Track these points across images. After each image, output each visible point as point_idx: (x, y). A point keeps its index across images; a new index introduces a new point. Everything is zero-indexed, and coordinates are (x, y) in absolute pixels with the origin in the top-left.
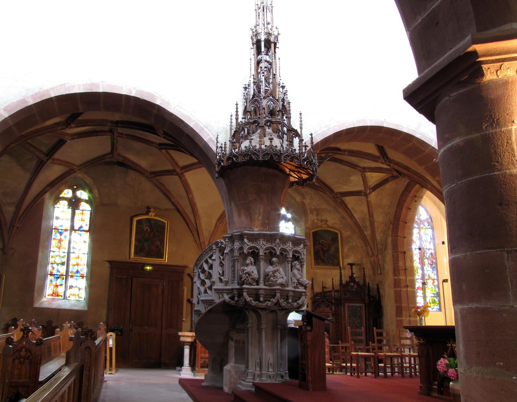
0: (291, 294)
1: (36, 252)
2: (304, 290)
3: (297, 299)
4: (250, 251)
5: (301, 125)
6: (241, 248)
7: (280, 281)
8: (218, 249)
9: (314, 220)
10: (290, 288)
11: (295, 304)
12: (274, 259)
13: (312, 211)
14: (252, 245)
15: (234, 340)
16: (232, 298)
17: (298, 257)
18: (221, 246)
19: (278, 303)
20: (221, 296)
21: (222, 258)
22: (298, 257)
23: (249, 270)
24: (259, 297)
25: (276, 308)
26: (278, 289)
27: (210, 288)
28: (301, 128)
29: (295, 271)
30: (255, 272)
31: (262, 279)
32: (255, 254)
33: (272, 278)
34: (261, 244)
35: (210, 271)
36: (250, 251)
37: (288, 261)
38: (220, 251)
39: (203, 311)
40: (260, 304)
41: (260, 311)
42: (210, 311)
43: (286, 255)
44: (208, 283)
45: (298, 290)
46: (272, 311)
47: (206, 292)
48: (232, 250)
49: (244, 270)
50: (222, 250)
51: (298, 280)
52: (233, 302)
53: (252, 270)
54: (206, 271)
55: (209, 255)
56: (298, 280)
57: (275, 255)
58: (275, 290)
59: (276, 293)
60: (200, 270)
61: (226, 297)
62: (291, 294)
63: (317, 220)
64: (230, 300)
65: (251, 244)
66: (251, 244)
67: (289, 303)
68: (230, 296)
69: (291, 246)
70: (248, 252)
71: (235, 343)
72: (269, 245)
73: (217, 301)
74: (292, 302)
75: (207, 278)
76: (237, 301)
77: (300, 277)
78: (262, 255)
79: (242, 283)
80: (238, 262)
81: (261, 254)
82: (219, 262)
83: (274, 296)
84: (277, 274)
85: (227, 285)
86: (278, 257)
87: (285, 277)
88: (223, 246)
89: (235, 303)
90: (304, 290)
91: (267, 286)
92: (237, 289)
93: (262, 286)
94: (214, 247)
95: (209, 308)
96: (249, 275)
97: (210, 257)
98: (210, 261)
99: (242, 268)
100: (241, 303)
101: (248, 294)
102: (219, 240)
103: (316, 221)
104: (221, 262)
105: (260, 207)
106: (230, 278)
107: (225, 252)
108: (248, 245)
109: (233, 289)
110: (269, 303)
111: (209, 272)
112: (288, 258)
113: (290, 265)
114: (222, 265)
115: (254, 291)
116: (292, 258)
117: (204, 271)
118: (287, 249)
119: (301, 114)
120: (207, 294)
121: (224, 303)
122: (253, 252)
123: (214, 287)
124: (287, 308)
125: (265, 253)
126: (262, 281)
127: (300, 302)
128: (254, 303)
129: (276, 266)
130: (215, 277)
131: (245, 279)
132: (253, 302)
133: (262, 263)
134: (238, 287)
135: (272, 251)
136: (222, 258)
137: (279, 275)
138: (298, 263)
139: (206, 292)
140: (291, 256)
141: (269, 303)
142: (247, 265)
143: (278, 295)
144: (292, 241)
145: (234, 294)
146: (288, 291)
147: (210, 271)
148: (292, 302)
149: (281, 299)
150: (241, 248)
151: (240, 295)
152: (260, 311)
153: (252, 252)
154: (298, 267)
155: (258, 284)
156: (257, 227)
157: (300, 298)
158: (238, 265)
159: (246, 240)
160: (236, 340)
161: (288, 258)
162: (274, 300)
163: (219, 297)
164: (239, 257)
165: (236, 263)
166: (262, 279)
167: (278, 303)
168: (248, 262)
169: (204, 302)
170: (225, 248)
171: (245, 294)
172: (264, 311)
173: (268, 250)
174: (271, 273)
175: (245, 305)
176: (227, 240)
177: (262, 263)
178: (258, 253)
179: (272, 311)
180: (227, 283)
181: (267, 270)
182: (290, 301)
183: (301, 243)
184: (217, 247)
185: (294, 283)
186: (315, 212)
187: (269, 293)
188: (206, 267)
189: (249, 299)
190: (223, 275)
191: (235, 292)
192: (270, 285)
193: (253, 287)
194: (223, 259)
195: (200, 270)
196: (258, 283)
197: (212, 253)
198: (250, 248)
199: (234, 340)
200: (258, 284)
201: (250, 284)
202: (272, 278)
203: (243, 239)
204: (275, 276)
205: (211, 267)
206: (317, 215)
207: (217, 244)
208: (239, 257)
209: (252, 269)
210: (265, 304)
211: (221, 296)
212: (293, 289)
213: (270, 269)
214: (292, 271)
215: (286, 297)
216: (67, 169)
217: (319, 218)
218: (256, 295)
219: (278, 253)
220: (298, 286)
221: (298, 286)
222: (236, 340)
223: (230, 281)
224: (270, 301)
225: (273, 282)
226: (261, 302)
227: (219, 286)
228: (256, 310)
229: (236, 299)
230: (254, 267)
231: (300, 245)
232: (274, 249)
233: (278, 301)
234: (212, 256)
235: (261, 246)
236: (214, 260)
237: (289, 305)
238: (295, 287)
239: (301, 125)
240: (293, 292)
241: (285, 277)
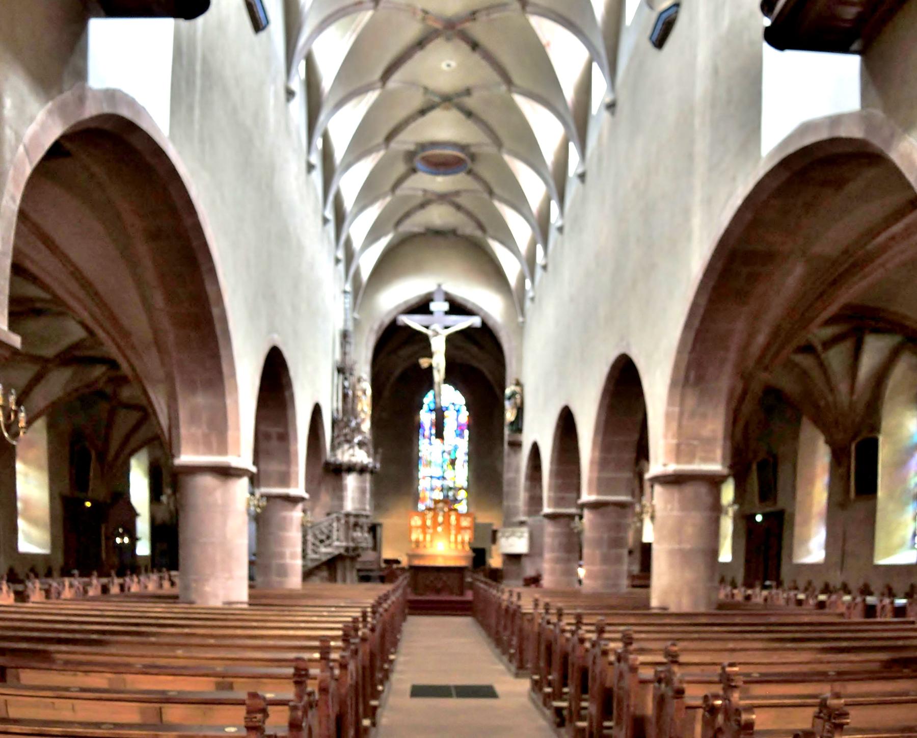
227: (336, 543)
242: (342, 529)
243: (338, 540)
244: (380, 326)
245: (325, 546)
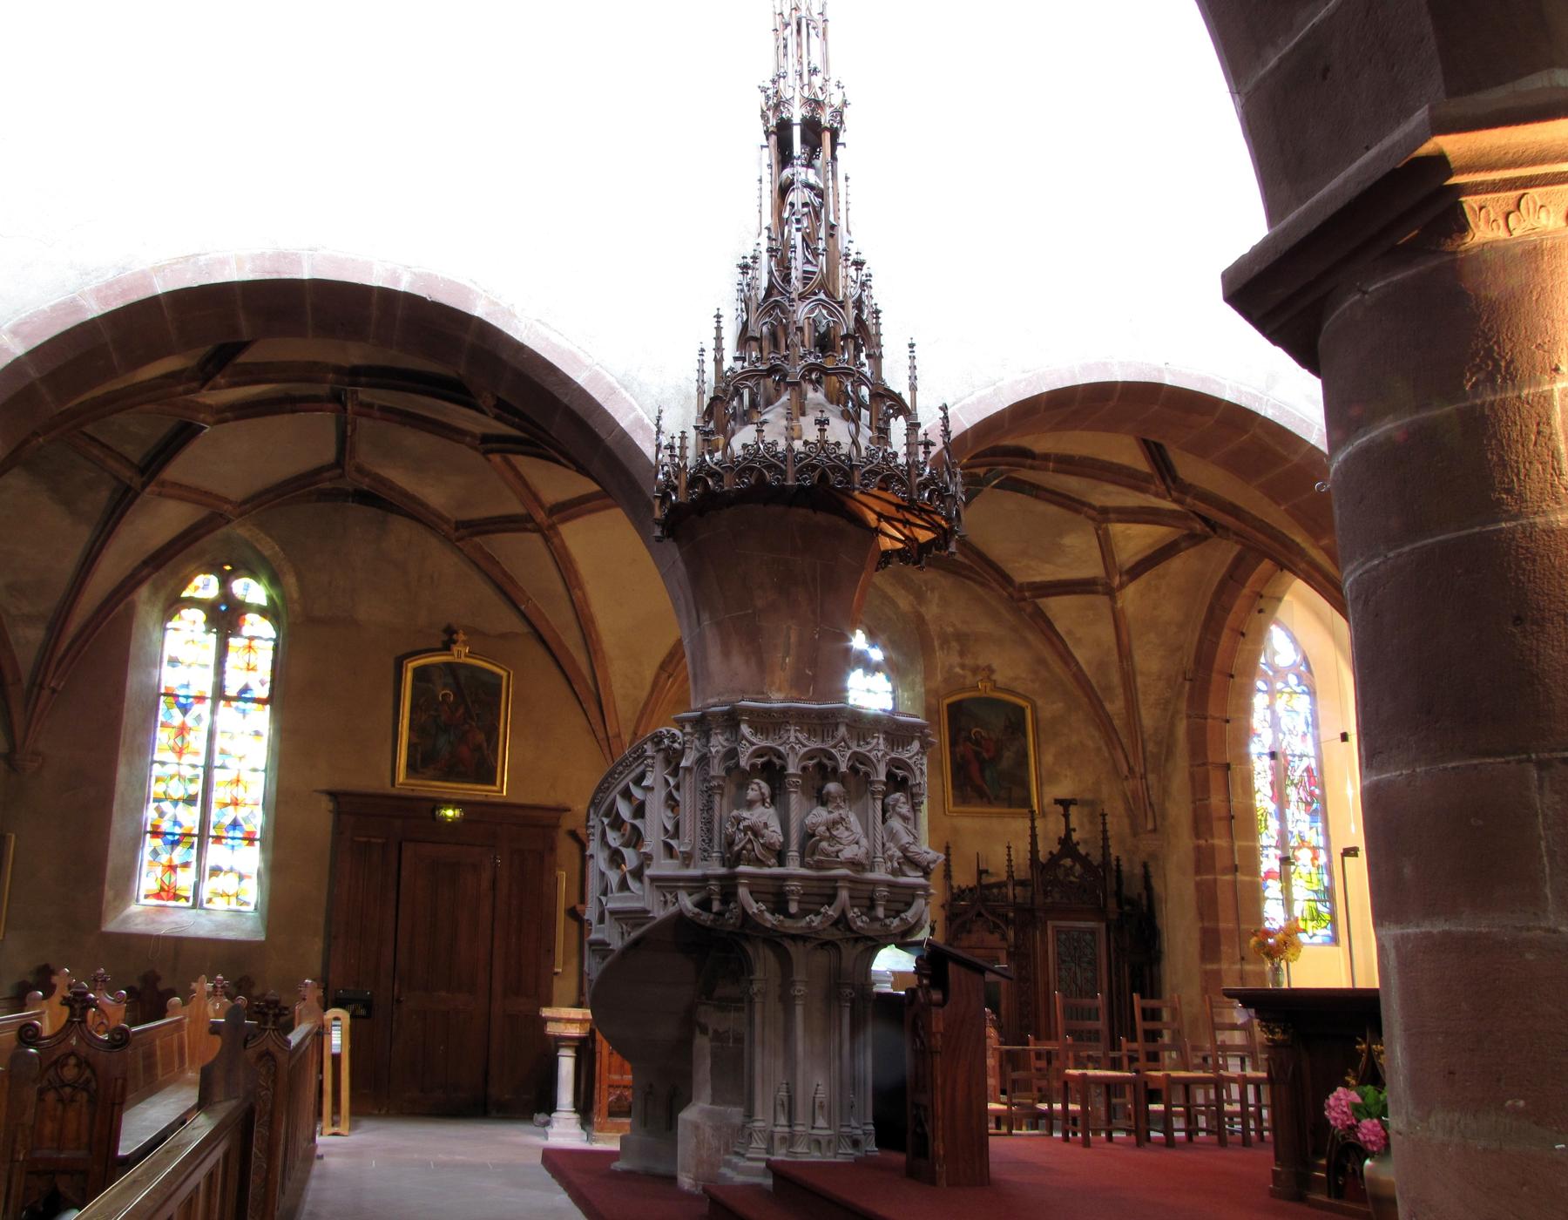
0: (883, 891)
2: (922, 881)
3: (900, 906)
4: (760, 761)
6: (732, 754)
7: (848, 852)
8: (661, 756)
10: (880, 874)
11: (896, 922)
12: (832, 787)
13: (945, 641)
14: (764, 744)
15: (711, 1032)
16: (704, 905)
17: (905, 779)
18: (669, 747)
19: (842, 921)
20: (669, 897)
21: (672, 781)
22: (905, 779)
23: (754, 819)
24: (787, 902)
25: (836, 935)
26: (844, 878)
27: (638, 874)
29: (896, 823)
30: (775, 825)
31: (794, 846)
32: (772, 771)
33: (824, 844)
34: (792, 739)
35: (637, 822)
36: (760, 761)
37: (873, 793)
38: (668, 761)
39: (617, 944)
40: (788, 923)
41: (787, 943)
42: (636, 943)
43: (867, 775)
44: (631, 857)
45: (902, 880)
46: (824, 945)
47: (623, 885)
48: (703, 760)
49: (739, 820)
50: (672, 759)
51: (904, 850)
52: (706, 918)
53: (764, 819)
54: (624, 821)
55: (633, 775)
56: (904, 850)
58: (835, 879)
59: (836, 889)
60: (606, 821)
61: (687, 902)
62: (883, 891)
63: (963, 666)
64: (697, 910)
65: (761, 742)
66: (761, 742)
67: (877, 919)
68: (696, 897)
69: (882, 747)
70: (753, 766)
71: (711, 1040)
72: (815, 744)
73: (660, 913)
74: (887, 917)
75: (627, 845)
76: (720, 914)
77: (911, 839)
78: (794, 775)
79: (733, 858)
80: (722, 795)
81: (791, 770)
82: (663, 794)
83: (831, 899)
84: (840, 832)
85: (688, 866)
86: (842, 779)
87: (864, 842)
88: (676, 745)
89: (714, 921)
90: (922, 881)
91: (810, 867)
92: (719, 878)
93: (793, 868)
94: (650, 749)
95: (634, 935)
96: (756, 834)
97: (638, 781)
98: (638, 793)
99: (735, 813)
100: (731, 918)
101: (751, 893)
102: (663, 730)
103: (958, 670)
104: (670, 796)
106: (699, 844)
107: (683, 764)
108: (752, 744)
109: (705, 878)
110: (817, 921)
111: (634, 827)
112: (872, 783)
113: (879, 804)
114: (672, 803)
115: (770, 882)
116: (885, 784)
117: (617, 823)
118: (871, 755)
120: (627, 894)
121: (680, 921)
122: (768, 766)
123: (648, 872)
124: (871, 934)
125: (804, 769)
126: (793, 853)
128: (770, 919)
129: (839, 807)
130: (653, 841)
131: (744, 848)
132: (768, 915)
133: (793, 797)
134: (722, 871)
135: (826, 761)
136: (672, 781)
137: (847, 833)
138: (903, 799)
139: (623, 885)
140: (883, 778)
141: (817, 921)
142: (750, 805)
143: (844, 895)
144: (885, 732)
145: (710, 893)
146: (875, 883)
147: (637, 822)
148: (887, 917)
149: (853, 906)
150: (732, 754)
151: (729, 895)
152: (787, 943)
153: (763, 764)
154: (905, 809)
155: (781, 863)
157: (909, 905)
158: (721, 805)
159: (745, 729)
160: (716, 1031)
161: (872, 783)
162: (831, 912)
163: (666, 902)
164: (724, 779)
165: (717, 798)
166: (794, 846)
167: (842, 921)
168: (752, 794)
170: (681, 754)
171: (743, 892)
172: (800, 943)
173: (811, 758)
174: (822, 828)
175: (742, 926)
176: (688, 729)
177: (794, 799)
178: (784, 768)
179: (824, 945)
180: (687, 859)
181: (810, 820)
182: (880, 912)
183: (913, 739)
184: (658, 751)
185: (891, 858)
186: (954, 644)
187: (815, 890)
188: (624, 810)
189: (754, 907)
190: (676, 834)
191: (714, 886)
192: (819, 866)
193: (766, 871)
194: (677, 787)
195: (606, 821)
196: (781, 859)
197: (642, 768)
198: (759, 753)
199: (711, 1032)
200: (781, 863)
201: (759, 862)
202: (824, 844)
203: (738, 725)
204: (833, 837)
205: (639, 811)
206: (962, 654)
207: (657, 740)
208: (724, 779)
209: (764, 816)
210: (803, 923)
211: (669, 897)
212: (890, 877)
213: (820, 815)
214: (884, 821)
215: (867, 903)
217: (969, 661)
218: (776, 896)
219: (843, 768)
220: (905, 868)
221: (905, 868)
222: (716, 1031)
223: (698, 854)
224: (818, 913)
225: (827, 855)
226: (791, 916)
227: (664, 867)
228: (775, 941)
229: (716, 906)
230: (772, 811)
231: (909, 744)
232: (832, 757)
233: (843, 913)
234: (642, 776)
235: (792, 748)
236: (649, 789)
237: (877, 925)
238: (894, 872)
240: (890, 885)
241: (864, 842)
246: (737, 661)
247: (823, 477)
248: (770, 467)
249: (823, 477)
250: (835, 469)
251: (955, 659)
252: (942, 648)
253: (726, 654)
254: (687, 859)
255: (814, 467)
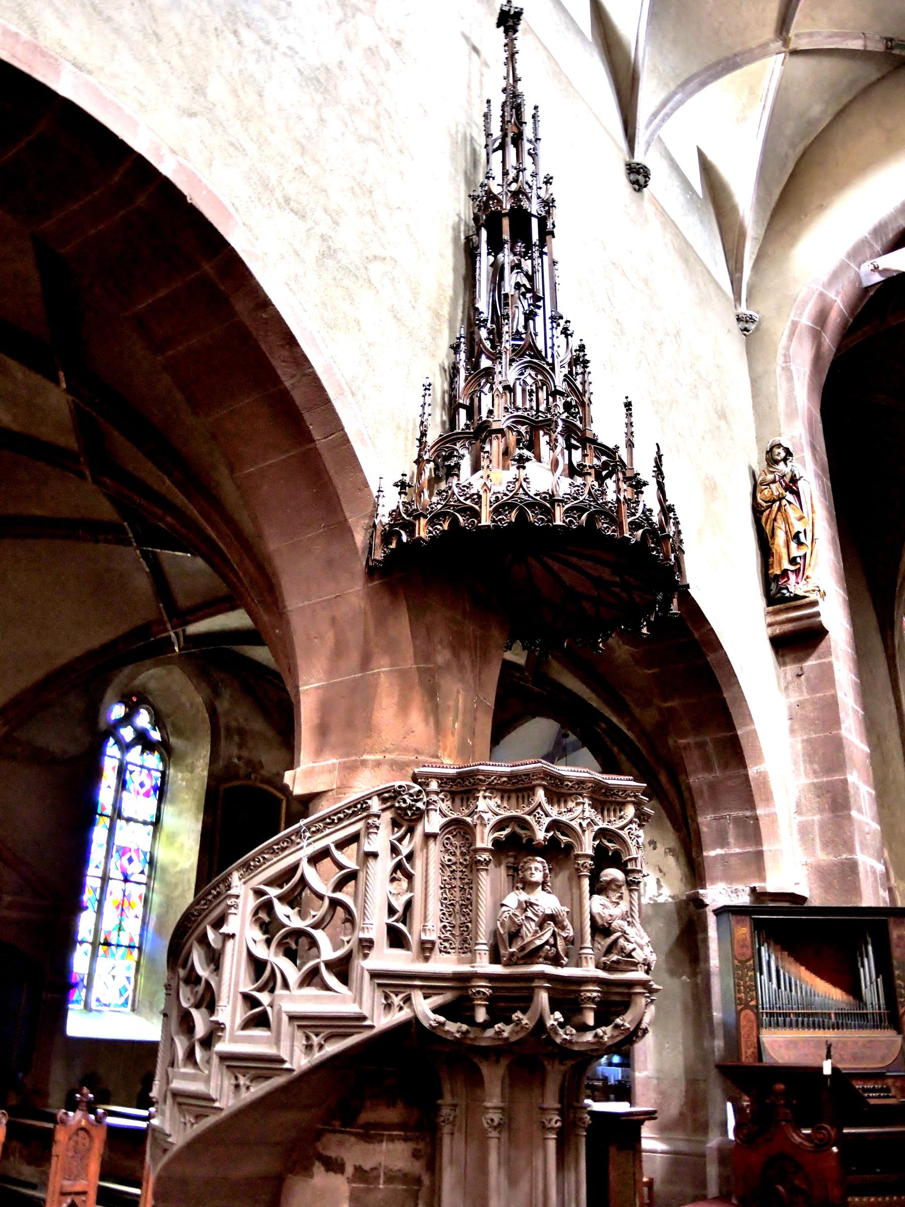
0: (593, 992)
1: (878, 809)
5: (630, 435)
9: (230, 758)
13: (229, 736)
15: (349, 1170)
17: (617, 853)
22: (617, 853)
24: (472, 1009)
28: (630, 445)
57: (532, 849)
59: (630, 995)
61: (424, 1007)
63: (239, 758)
71: (350, 1181)
73: (382, 1021)
78: (485, 850)
83: (525, 1002)
85: (427, 959)
103: (236, 760)
105: (458, 692)
110: (507, 1030)
118: (574, 824)
119: (628, 405)
127: (626, 1021)
128: (564, 1035)
140: (590, 852)
141: (507, 1030)
148: (598, 1025)
156: (450, 756)
158: (488, 882)
160: (358, 1169)
169: (304, 1022)
180: (426, 949)
186: (236, 738)
199: (349, 1170)
206: (241, 746)
216: (224, 589)
217: (245, 754)
218: (567, 996)
219: (541, 835)
222: (358, 1169)
224: (508, 1021)
227: (387, 959)
232: (523, 823)
233: (541, 1021)
237: (589, 1037)
239: (630, 435)
242: (431, 864)
243: (397, 939)
244: (821, 318)
245: (311, 978)
246: (416, 718)
247: (522, 515)
248: (465, 510)
249: (522, 515)
250: (532, 505)
251: (235, 751)
252: (226, 737)
253: (404, 708)
254: (426, 949)
255: (512, 506)
